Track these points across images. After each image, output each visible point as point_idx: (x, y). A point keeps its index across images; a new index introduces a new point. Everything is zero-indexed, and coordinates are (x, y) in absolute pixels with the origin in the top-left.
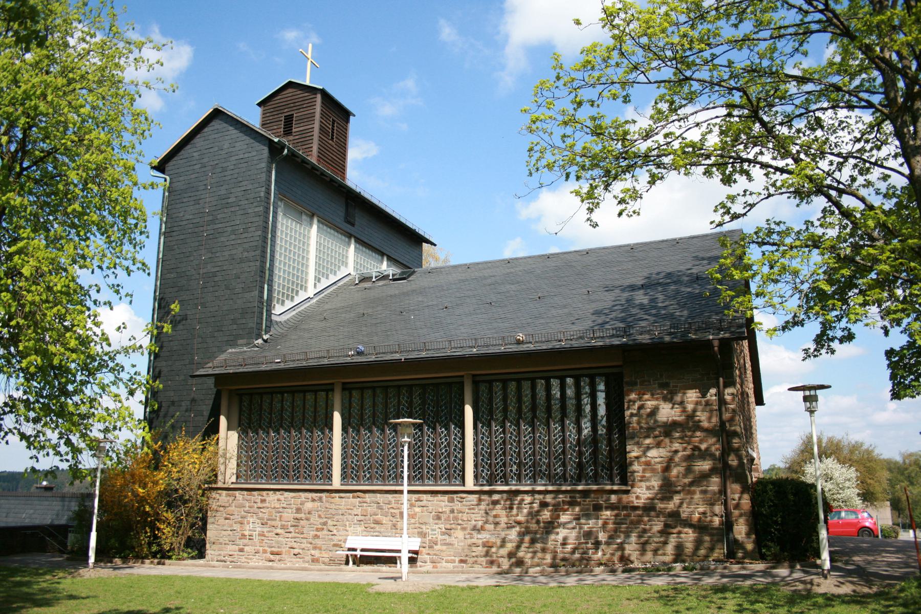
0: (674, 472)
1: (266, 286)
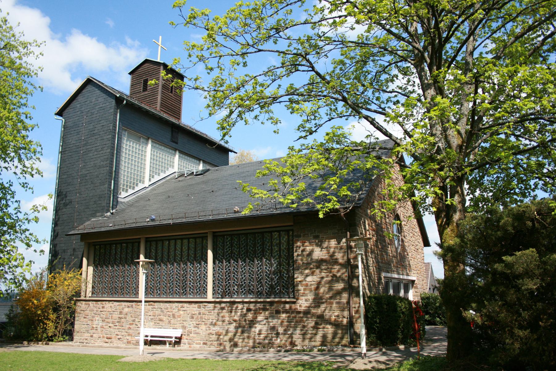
0: (322, 290)
1: (113, 182)
